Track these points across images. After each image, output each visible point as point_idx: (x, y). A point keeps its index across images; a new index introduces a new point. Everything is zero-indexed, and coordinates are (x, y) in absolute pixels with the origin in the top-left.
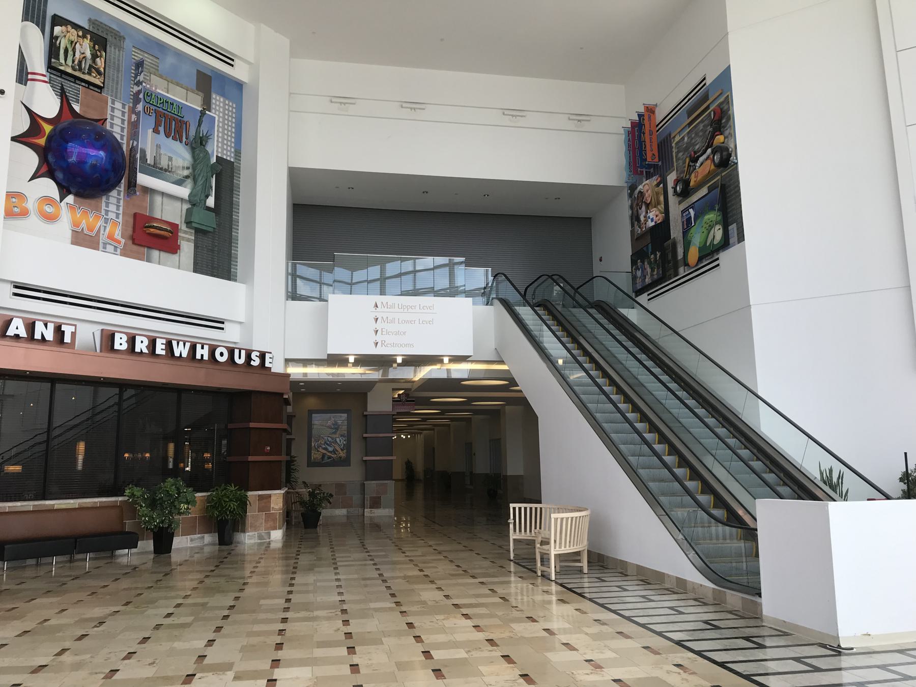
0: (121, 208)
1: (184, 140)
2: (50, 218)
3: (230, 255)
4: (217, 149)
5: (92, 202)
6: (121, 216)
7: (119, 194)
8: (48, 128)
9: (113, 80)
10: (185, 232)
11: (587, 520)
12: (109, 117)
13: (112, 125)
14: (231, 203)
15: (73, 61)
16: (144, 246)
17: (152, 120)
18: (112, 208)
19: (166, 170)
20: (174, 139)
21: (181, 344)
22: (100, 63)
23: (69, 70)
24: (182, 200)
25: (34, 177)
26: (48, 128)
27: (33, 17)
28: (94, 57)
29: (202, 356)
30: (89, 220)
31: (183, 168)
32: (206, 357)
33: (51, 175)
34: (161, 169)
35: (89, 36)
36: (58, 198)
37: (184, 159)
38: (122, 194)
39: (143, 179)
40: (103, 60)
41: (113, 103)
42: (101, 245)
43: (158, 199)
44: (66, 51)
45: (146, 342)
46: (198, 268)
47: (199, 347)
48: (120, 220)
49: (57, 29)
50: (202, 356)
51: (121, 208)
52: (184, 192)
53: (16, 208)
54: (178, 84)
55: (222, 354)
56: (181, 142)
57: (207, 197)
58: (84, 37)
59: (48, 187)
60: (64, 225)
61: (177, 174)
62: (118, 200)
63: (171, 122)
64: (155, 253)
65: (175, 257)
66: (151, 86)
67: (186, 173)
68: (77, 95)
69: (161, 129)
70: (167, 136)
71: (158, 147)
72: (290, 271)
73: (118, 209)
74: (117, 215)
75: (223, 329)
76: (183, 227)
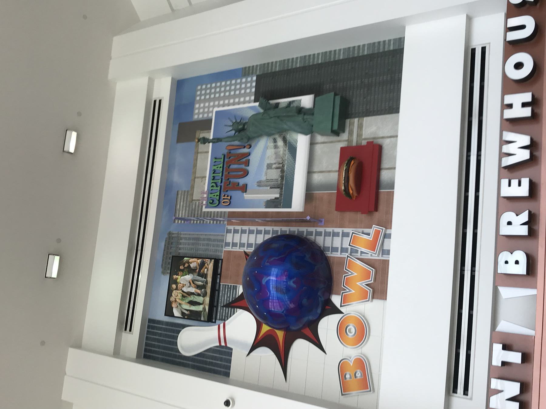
0: (337, 230)
1: (246, 150)
2: (362, 332)
3: (371, 57)
4: (247, 106)
5: (335, 269)
6: (346, 230)
7: (319, 234)
8: (265, 328)
9: (208, 245)
10: (351, 133)
11: (336, 195)
12: (242, 250)
13: (250, 245)
14: (304, 69)
15: (199, 295)
16: (377, 194)
17: (236, 194)
18: (337, 242)
19: (283, 171)
20: (247, 163)
21: (506, 149)
22: (194, 263)
23: (207, 299)
24: (312, 144)
25: (319, 345)
26: (265, 328)
27: (173, 331)
28: (191, 271)
29: (524, 105)
30: (355, 276)
31: (276, 147)
32: (527, 97)
33: (313, 326)
34: (282, 177)
35: (175, 277)
36: (341, 315)
37: (266, 148)
38: (319, 229)
39: (298, 203)
40: (191, 260)
41: (227, 244)
42: (385, 258)
43: (317, 178)
44: (192, 303)
45: (509, 216)
46: (393, 108)
47: (509, 114)
48: (350, 230)
49: (176, 313)
50: (524, 105)
51: (337, 230)
52: (302, 142)
53: (358, 378)
54: (195, 165)
55: (519, 66)
56: (249, 154)
57: (300, 110)
58: (176, 282)
59: (327, 326)
60: (369, 309)
61: (284, 154)
62: (327, 234)
63: (230, 175)
64: (385, 175)
65: (386, 144)
66: (203, 199)
67: (280, 143)
68: (229, 288)
69: (242, 181)
70: (246, 173)
71: (260, 184)
72: (215, 309)
73: (337, 234)
74: (345, 235)
75: (484, 49)
76: (345, 136)
